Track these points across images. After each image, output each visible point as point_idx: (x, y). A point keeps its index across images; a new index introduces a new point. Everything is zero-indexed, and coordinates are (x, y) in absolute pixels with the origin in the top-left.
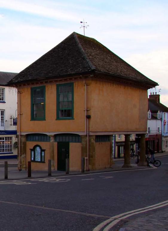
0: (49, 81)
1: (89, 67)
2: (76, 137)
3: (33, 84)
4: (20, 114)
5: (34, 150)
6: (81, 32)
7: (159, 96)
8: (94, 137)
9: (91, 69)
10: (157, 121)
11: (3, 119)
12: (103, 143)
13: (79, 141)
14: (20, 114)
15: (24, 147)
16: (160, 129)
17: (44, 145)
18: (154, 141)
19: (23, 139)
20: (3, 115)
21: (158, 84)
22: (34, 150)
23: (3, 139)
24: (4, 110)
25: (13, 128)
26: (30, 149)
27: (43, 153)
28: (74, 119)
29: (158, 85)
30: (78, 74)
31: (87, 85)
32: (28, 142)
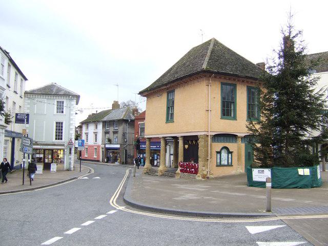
5: (219, 153)
27: (230, 155)
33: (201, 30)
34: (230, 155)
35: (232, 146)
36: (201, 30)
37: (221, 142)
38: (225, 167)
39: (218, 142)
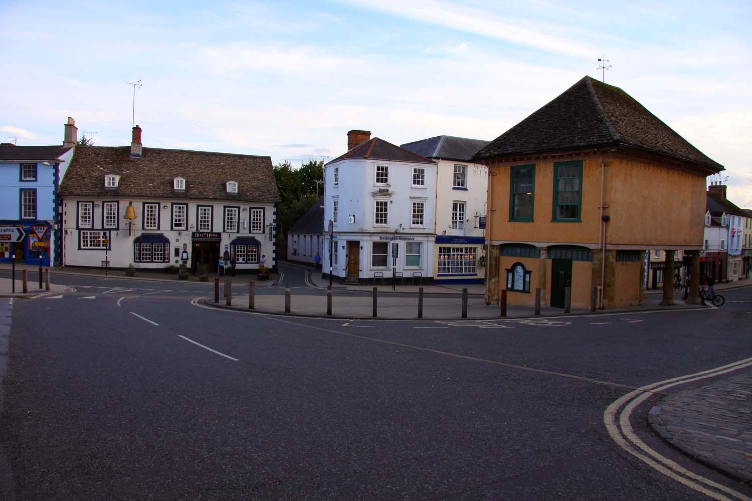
1: (610, 135)
2: (584, 252)
3: (515, 160)
4: (492, 211)
5: (512, 270)
6: (597, 76)
7: (725, 187)
8: (614, 253)
9: (612, 138)
14: (492, 211)
15: (496, 264)
16: (725, 243)
18: (714, 263)
20: (463, 211)
21: (725, 168)
22: (512, 270)
23: (462, 251)
24: (466, 202)
25: (479, 233)
27: (527, 276)
29: (725, 170)
31: (605, 166)
33: (600, 60)
34: (527, 276)
35: (530, 263)
36: (600, 60)
37: (511, 255)
38: (518, 293)
39: (507, 255)
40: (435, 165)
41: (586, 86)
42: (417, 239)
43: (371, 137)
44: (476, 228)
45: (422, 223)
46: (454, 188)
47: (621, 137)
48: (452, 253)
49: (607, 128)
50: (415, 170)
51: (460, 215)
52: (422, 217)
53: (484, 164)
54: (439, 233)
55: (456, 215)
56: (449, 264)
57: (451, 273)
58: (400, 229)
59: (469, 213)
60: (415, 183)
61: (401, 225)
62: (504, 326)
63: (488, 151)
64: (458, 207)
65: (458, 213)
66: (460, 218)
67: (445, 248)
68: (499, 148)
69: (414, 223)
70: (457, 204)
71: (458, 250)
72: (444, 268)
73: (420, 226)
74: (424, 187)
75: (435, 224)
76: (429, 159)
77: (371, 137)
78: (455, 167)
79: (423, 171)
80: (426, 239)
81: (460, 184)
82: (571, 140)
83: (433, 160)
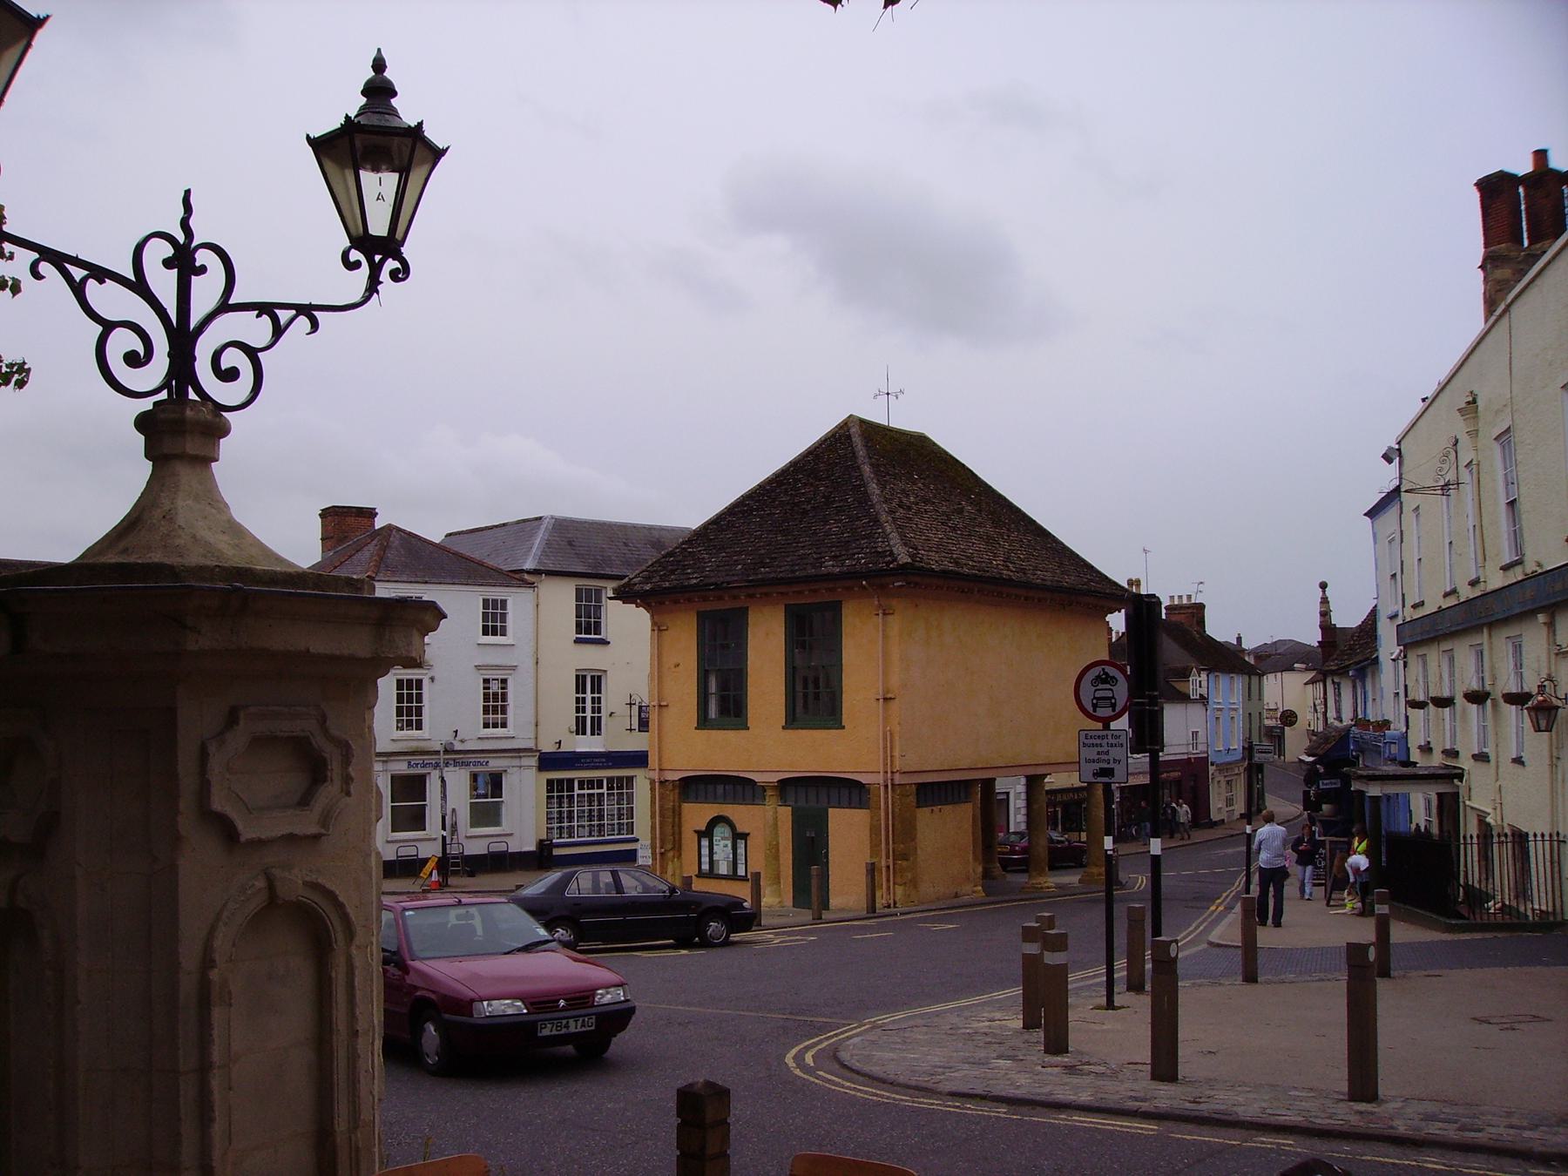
0: (761, 594)
1: (892, 553)
2: (850, 791)
3: (705, 599)
4: (660, 706)
5: (707, 833)
7: (1201, 607)
9: (895, 560)
10: (1189, 705)
11: (599, 708)
12: (947, 808)
13: (862, 805)
14: (660, 706)
17: (743, 815)
19: (673, 796)
20: (599, 692)
22: (707, 833)
23: (600, 787)
24: (605, 671)
25: (635, 742)
26: (696, 831)
27: (741, 844)
28: (843, 728)
30: (852, 576)
31: (884, 614)
32: (686, 807)
40: (531, 591)
41: (849, 437)
42: (495, 764)
43: (379, 523)
44: (631, 730)
45: (504, 725)
46: (577, 641)
47: (912, 556)
48: (577, 791)
49: (886, 536)
50: (486, 602)
51: (593, 702)
52: (504, 711)
53: (641, 606)
54: (548, 747)
55: (584, 702)
56: (570, 819)
57: (576, 839)
58: (455, 742)
59: (614, 698)
60: (485, 632)
61: (456, 732)
62: (1271, 889)
63: (647, 580)
64: (589, 683)
65: (589, 696)
66: (593, 708)
67: (560, 781)
68: (673, 572)
69: (486, 726)
70: (584, 677)
71: (591, 783)
72: (560, 828)
73: (499, 731)
74: (509, 642)
75: (537, 725)
76: (517, 576)
77: (379, 523)
78: (579, 592)
79: (504, 603)
80: (516, 762)
81: (589, 627)
82: (817, 559)
83: (526, 576)
